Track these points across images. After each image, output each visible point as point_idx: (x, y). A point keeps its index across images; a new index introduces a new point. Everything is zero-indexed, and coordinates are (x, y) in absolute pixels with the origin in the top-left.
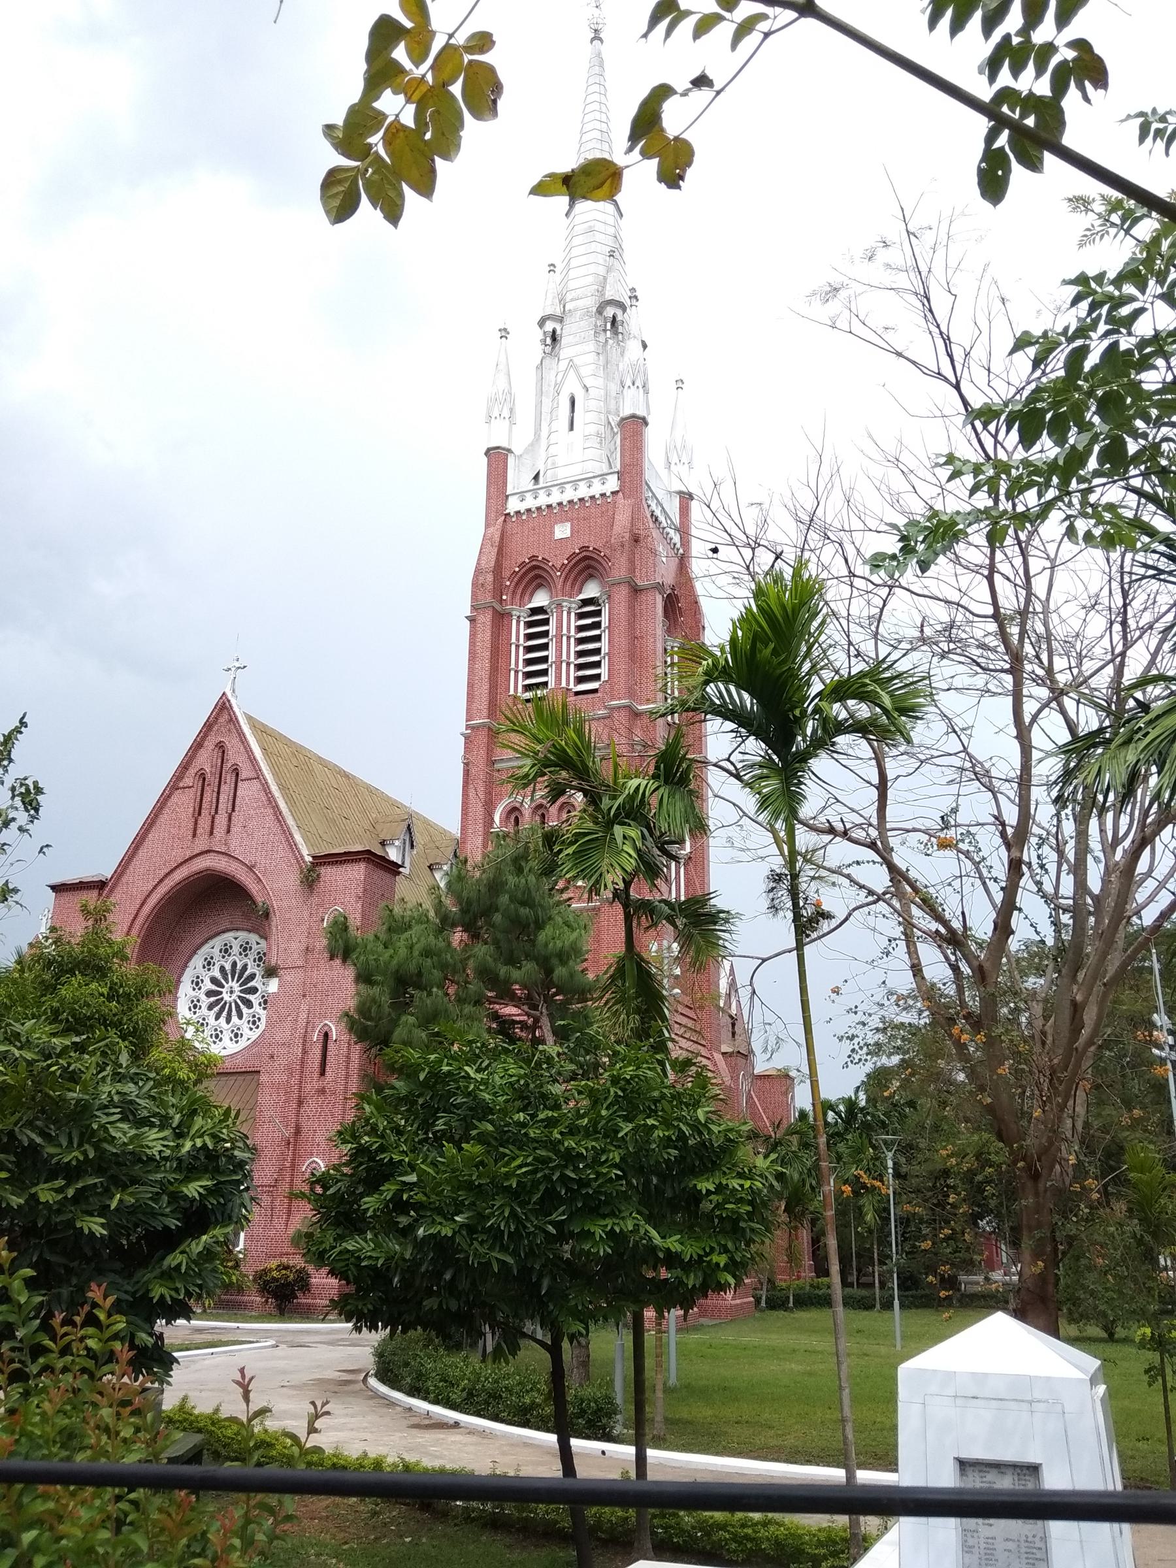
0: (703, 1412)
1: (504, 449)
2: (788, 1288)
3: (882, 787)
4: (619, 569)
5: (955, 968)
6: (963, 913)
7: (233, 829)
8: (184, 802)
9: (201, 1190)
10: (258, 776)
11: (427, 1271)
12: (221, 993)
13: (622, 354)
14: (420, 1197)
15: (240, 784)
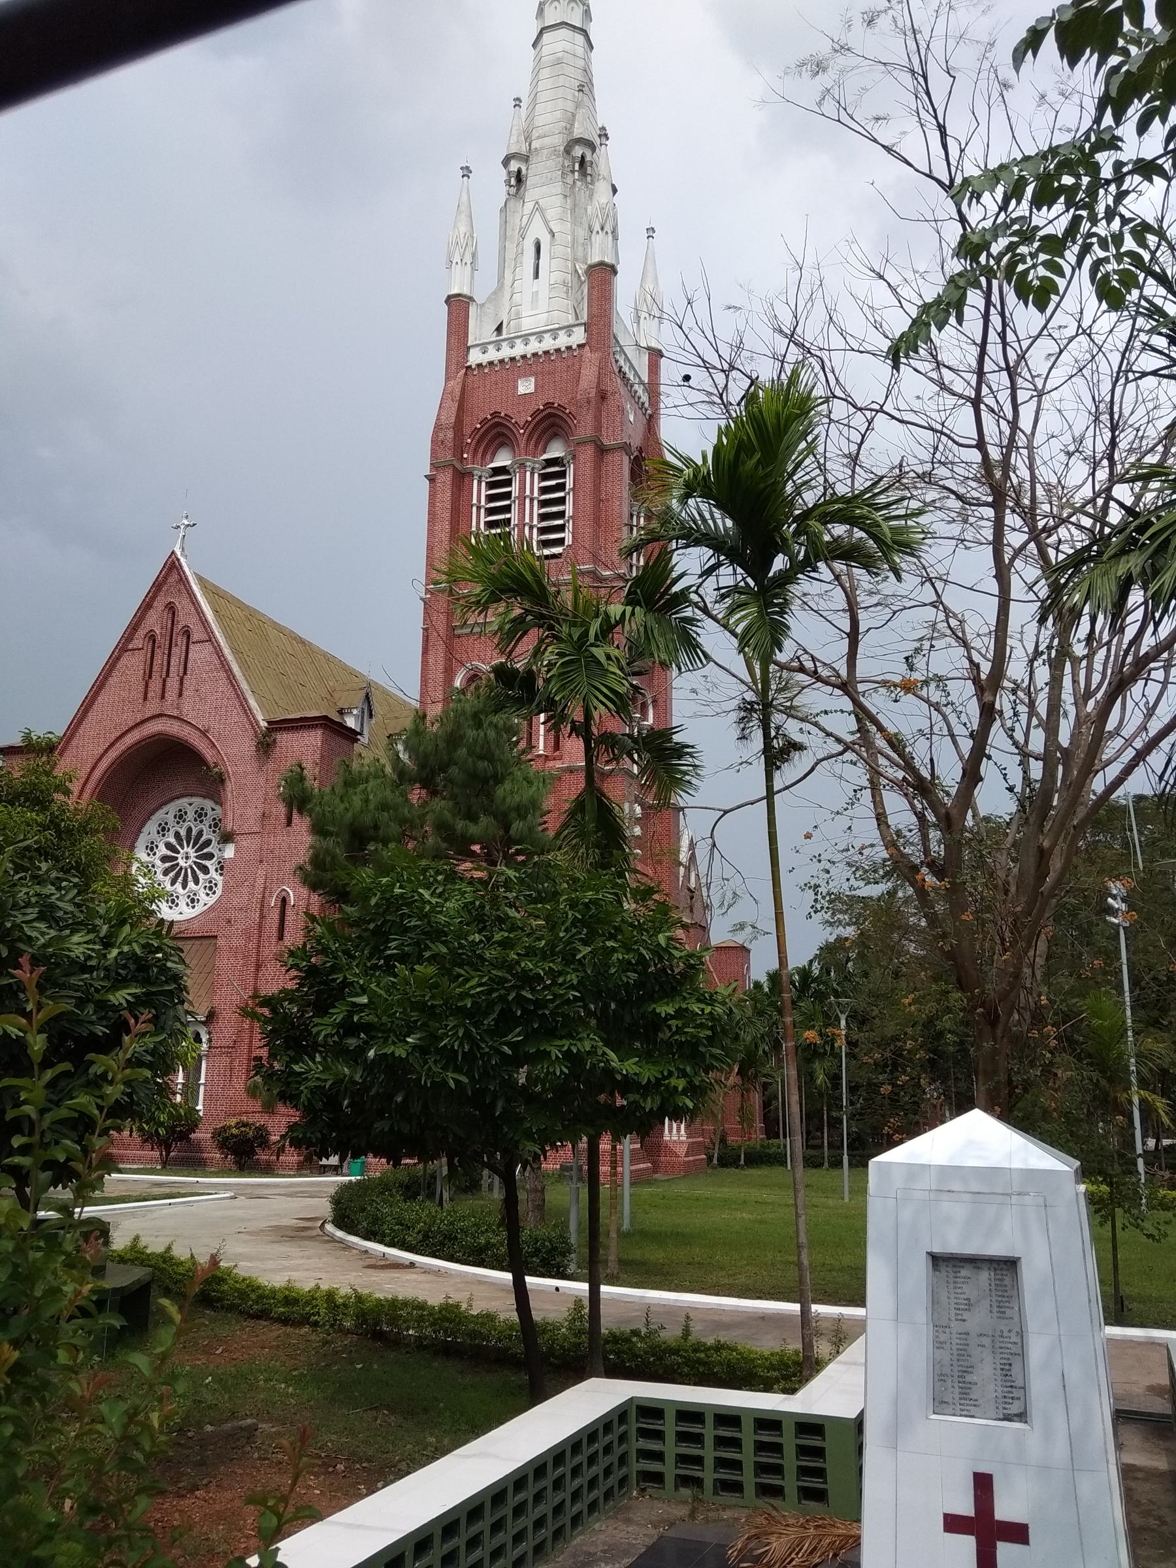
0: (655, 1254)
1: (465, 296)
2: (740, 1147)
3: (854, 637)
4: (584, 428)
5: (921, 817)
6: (932, 760)
7: (185, 693)
8: (133, 664)
9: (129, 998)
10: (210, 639)
11: (378, 1093)
12: (177, 858)
13: (591, 196)
14: (372, 1019)
15: (191, 646)
